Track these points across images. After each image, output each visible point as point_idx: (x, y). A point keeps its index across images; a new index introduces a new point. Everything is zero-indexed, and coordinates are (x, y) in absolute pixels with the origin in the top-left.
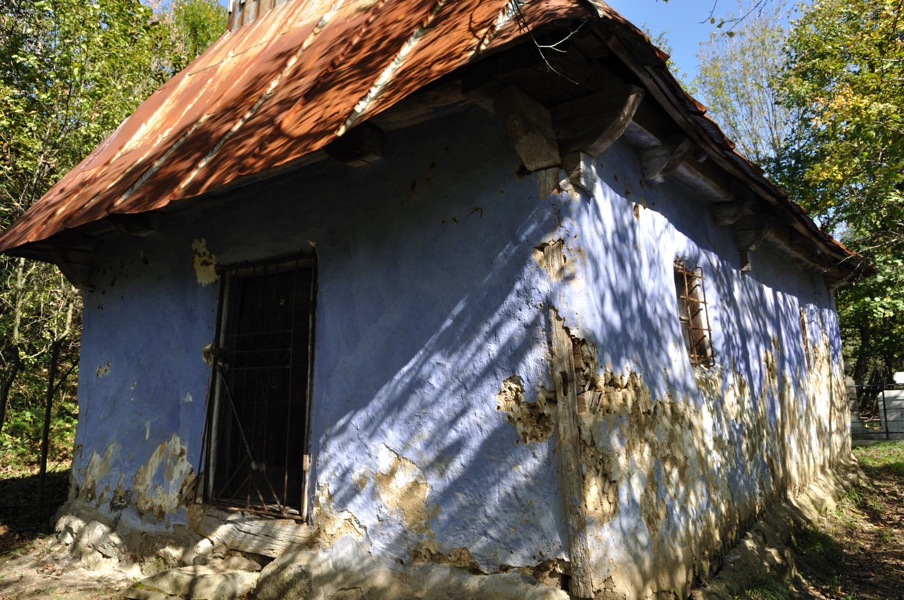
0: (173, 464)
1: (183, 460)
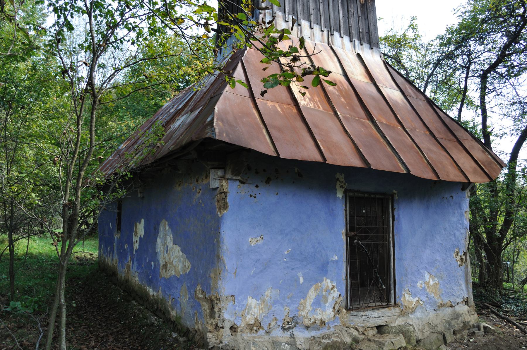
0: (327, 294)
1: (334, 291)
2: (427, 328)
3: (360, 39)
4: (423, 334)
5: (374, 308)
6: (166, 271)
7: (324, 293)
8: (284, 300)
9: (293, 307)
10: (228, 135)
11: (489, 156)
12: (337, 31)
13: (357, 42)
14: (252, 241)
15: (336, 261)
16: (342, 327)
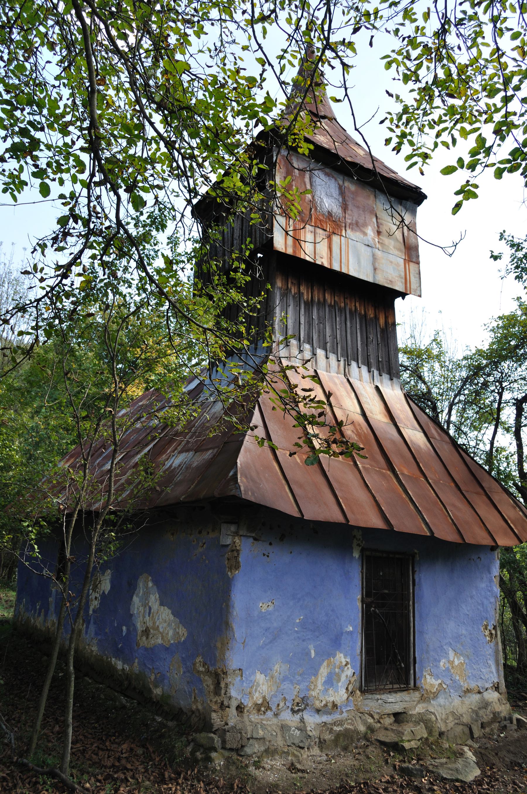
1: (348, 668)
2: (451, 718)
3: (379, 370)
4: (446, 726)
5: (391, 691)
6: (147, 638)
7: (337, 670)
8: (294, 677)
9: (303, 686)
10: (253, 494)
11: (521, 513)
12: (354, 360)
13: (376, 373)
14: (263, 606)
15: (351, 633)
16: (356, 712)
